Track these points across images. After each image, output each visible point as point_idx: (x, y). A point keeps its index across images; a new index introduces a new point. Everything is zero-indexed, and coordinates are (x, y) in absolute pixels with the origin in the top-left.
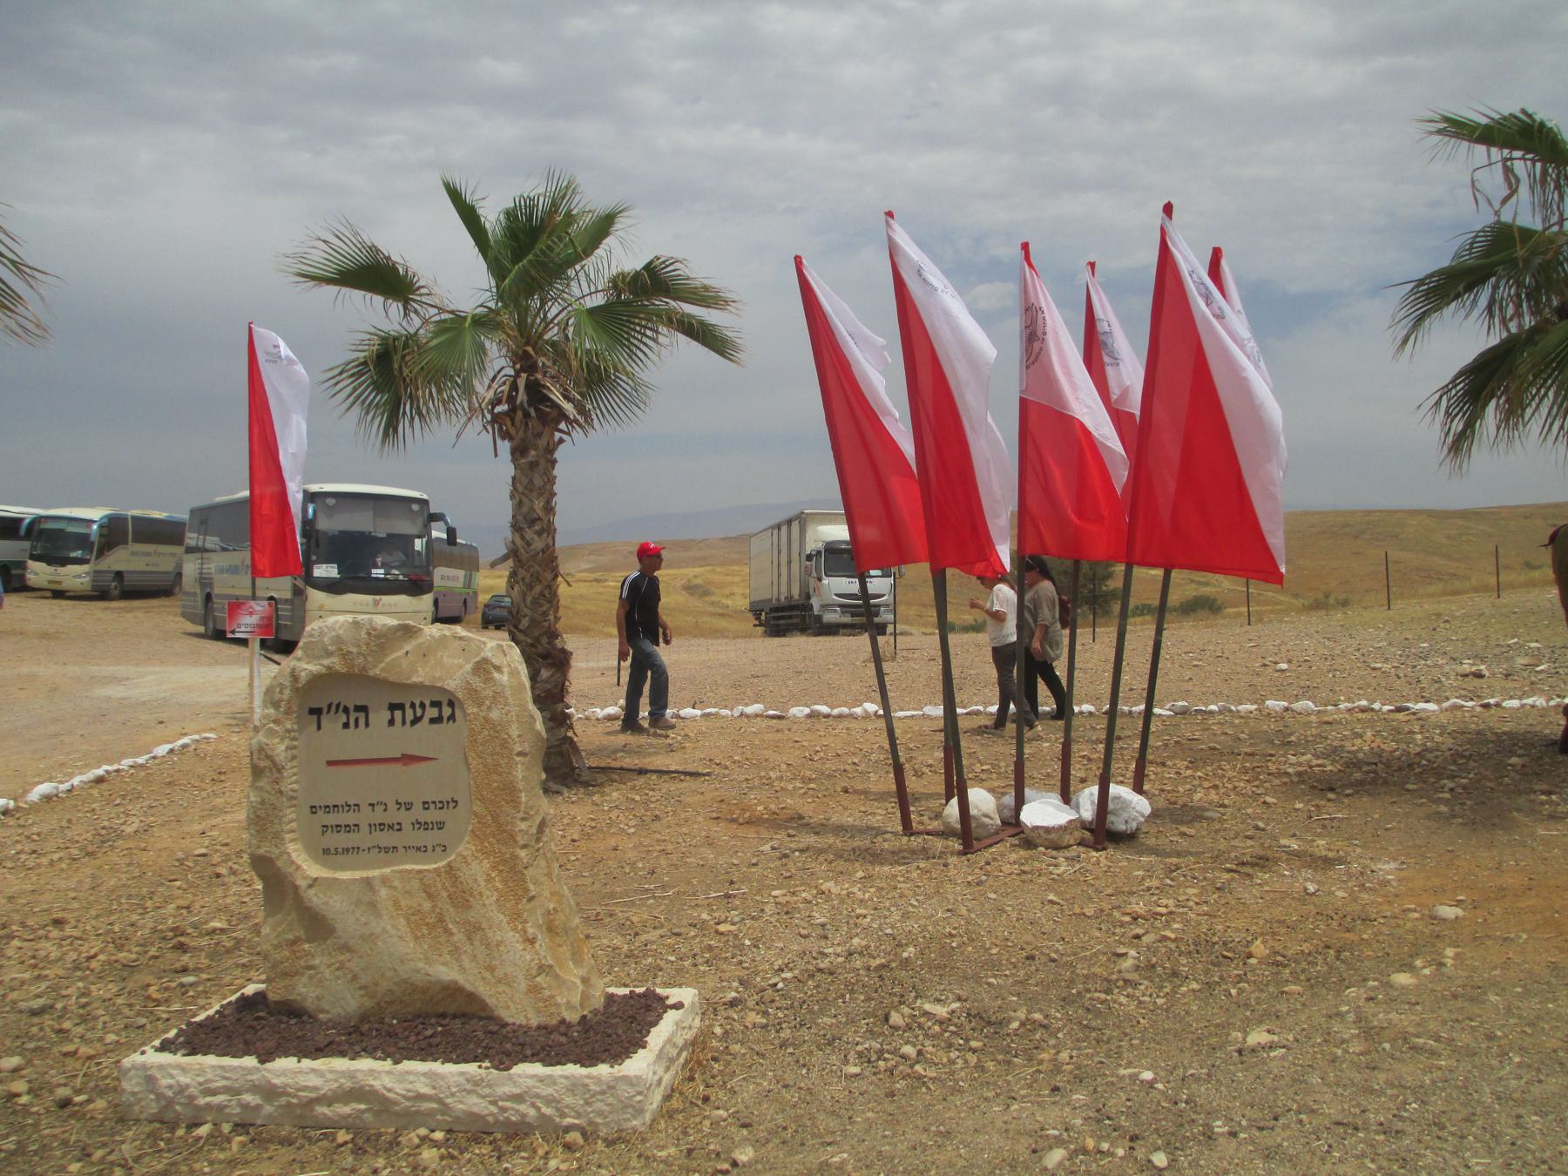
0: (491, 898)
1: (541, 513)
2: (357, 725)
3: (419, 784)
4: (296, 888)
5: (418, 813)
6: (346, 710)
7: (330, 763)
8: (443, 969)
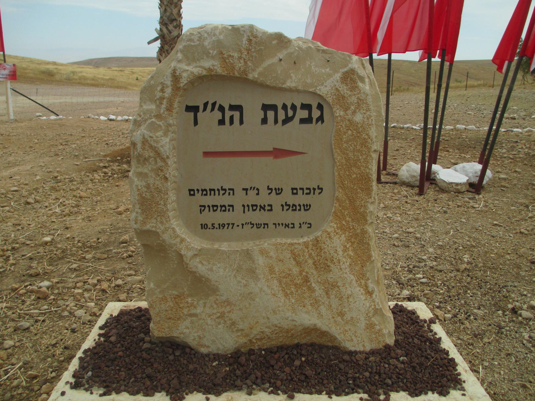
0: (346, 263)
1: (176, 16)
5: (287, 197)
6: (222, 109)
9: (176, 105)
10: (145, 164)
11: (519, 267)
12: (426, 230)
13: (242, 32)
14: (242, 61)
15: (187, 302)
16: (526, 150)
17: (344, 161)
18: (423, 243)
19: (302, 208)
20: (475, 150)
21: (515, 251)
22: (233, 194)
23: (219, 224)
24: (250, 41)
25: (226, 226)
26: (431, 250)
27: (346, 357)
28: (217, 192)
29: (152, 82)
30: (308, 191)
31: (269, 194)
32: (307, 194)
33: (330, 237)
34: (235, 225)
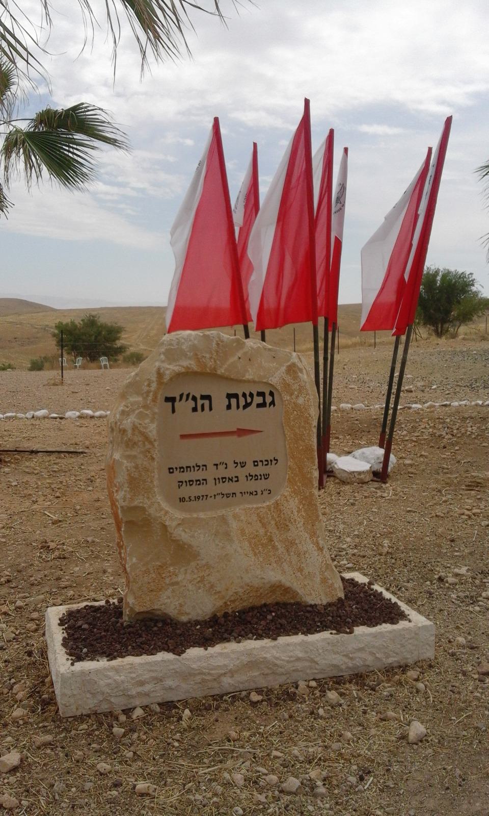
2: (203, 409)
3: (248, 448)
4: (165, 527)
5: (250, 469)
6: (194, 398)
7: (183, 437)
8: (272, 573)
9: (159, 396)
10: (134, 448)
11: (440, 546)
12: (337, 523)
13: (212, 338)
14: (212, 360)
15: (169, 572)
16: (431, 430)
17: (292, 436)
18: (338, 534)
19: (263, 477)
20: (370, 434)
21: (434, 533)
22: (206, 469)
23: (195, 497)
24: (218, 344)
25: (201, 498)
26: (348, 539)
27: (309, 609)
28: (192, 469)
29: (138, 378)
30: (267, 463)
31: (236, 467)
32: (266, 465)
33: (287, 501)
34: (208, 497)
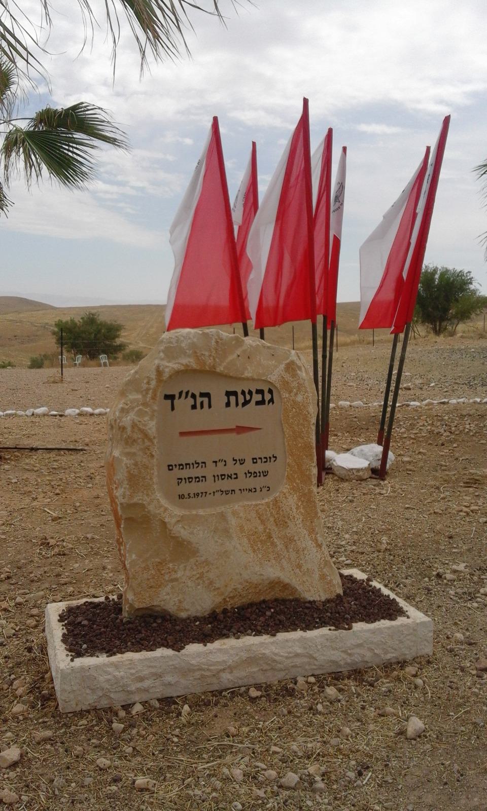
2: (202, 407)
3: (247, 446)
4: (164, 524)
5: (249, 466)
6: (193, 396)
7: (182, 434)
8: (270, 570)
9: (158, 394)
10: (133, 445)
11: (438, 543)
12: (336, 520)
13: (211, 336)
14: (211, 358)
15: (169, 568)
16: (429, 427)
17: (291, 433)
18: (336, 531)
19: (262, 474)
20: (368, 432)
21: (432, 530)
22: (205, 466)
23: (194, 494)
24: (217, 342)
25: (201, 494)
26: (347, 536)
27: (307, 605)
28: (191, 466)
29: (137, 376)
30: (266, 460)
31: (235, 464)
32: (265, 462)
33: (286, 497)
34: (208, 494)
